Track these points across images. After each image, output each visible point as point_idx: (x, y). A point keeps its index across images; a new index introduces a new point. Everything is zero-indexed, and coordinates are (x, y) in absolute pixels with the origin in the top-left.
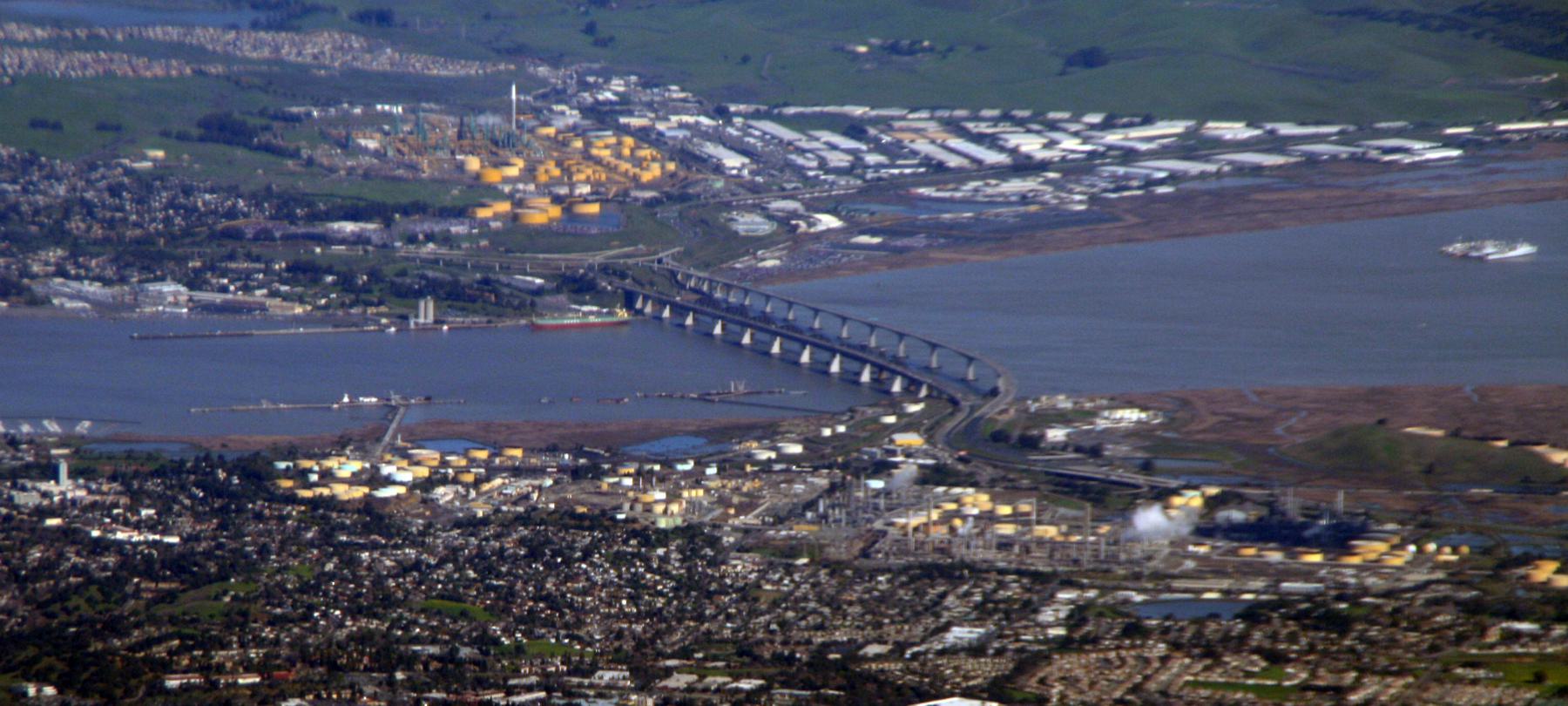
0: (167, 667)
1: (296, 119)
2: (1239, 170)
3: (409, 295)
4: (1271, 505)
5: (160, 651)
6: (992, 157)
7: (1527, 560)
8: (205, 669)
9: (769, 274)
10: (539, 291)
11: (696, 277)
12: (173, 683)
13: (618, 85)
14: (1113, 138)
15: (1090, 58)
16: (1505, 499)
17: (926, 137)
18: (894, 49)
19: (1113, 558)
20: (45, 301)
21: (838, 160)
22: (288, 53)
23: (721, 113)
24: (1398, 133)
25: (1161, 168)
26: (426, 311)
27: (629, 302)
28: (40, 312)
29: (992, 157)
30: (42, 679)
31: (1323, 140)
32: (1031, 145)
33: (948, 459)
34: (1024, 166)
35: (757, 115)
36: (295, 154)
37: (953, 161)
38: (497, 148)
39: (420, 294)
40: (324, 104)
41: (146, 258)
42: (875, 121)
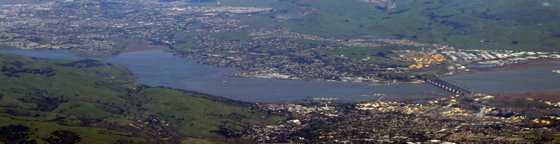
0: (320, 135)
1: (392, 53)
2: (529, 59)
3: (393, 79)
4: (500, 111)
5: (321, 133)
6: (493, 57)
7: (534, 119)
8: (326, 135)
9: (450, 75)
10: (413, 78)
11: (437, 76)
12: (320, 137)
13: (444, 47)
14: (513, 55)
15: (515, 43)
16: (538, 110)
17: (485, 55)
18: (486, 41)
19: (472, 118)
20: (341, 80)
21: (470, 58)
22: (397, 43)
23: (457, 51)
24: (556, 54)
25: (516, 59)
26: (395, 81)
27: (425, 80)
28: (340, 82)
29: (493, 57)
30: (302, 137)
31: (543, 55)
32: (500, 56)
33: (458, 103)
34: (497, 59)
35: (462, 51)
36: (389, 58)
37: (487, 58)
38: (420, 56)
39: (394, 79)
40: (397, 50)
41: (358, 74)
42: (478, 52)
